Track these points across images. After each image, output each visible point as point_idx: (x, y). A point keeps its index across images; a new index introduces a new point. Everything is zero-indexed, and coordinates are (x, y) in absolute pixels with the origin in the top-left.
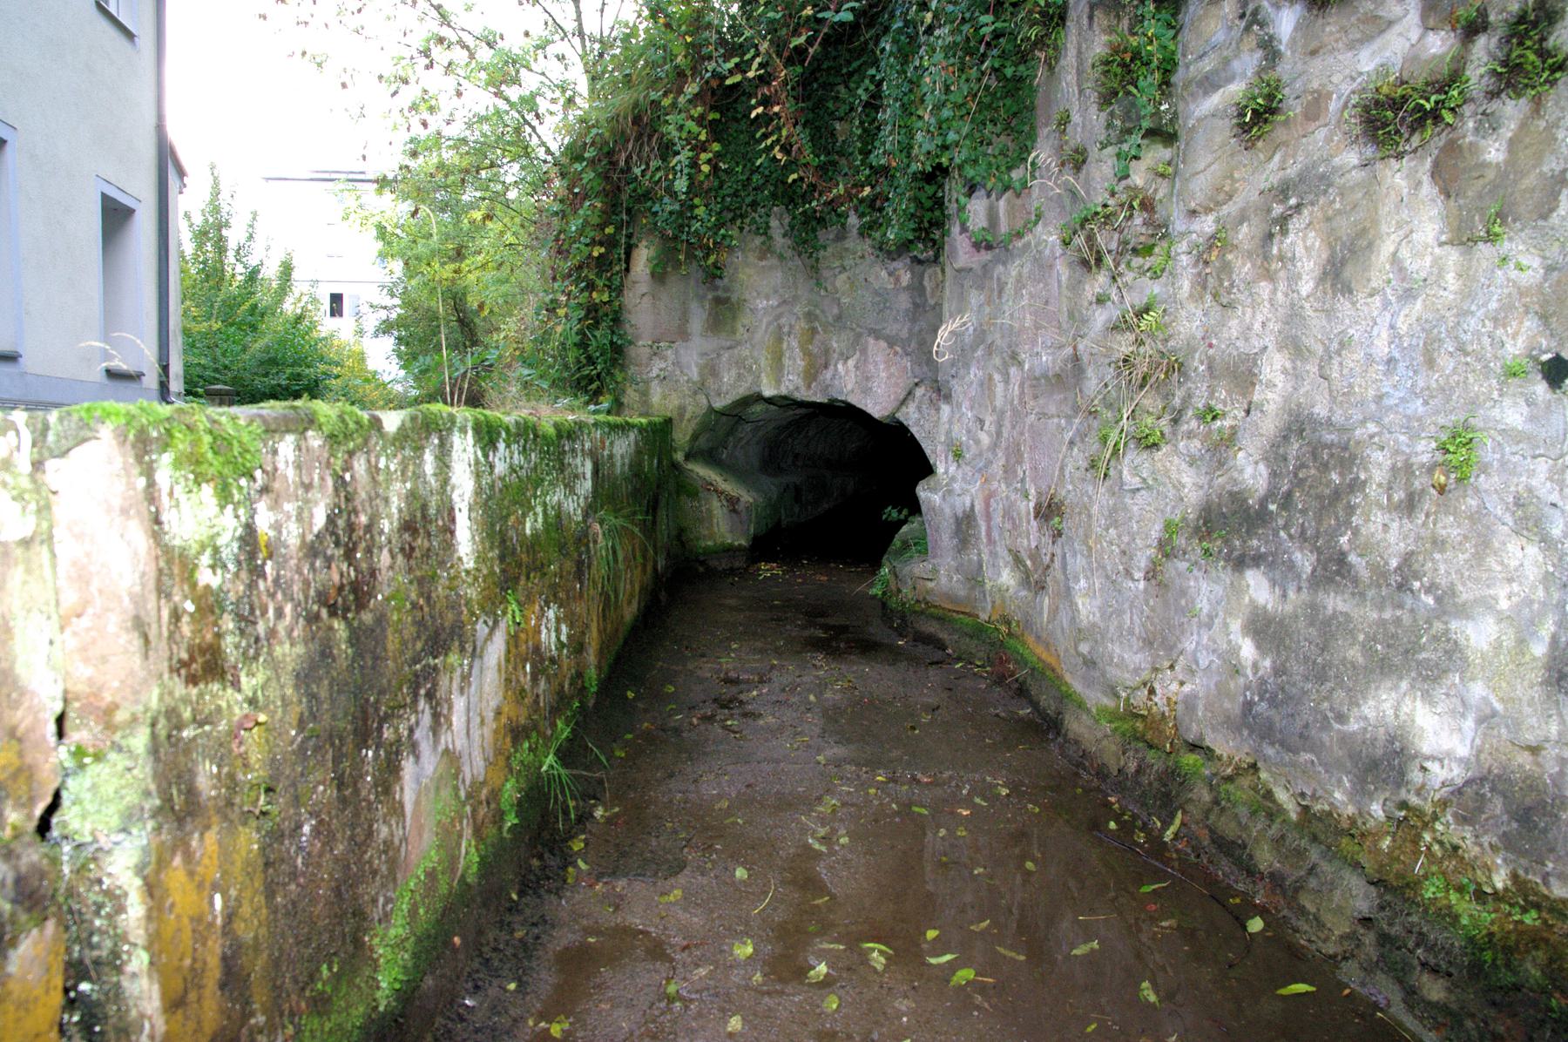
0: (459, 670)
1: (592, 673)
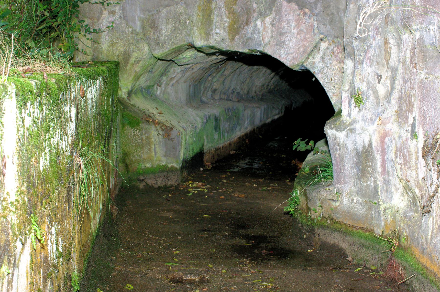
0: (7, 277)
1: (75, 274)
